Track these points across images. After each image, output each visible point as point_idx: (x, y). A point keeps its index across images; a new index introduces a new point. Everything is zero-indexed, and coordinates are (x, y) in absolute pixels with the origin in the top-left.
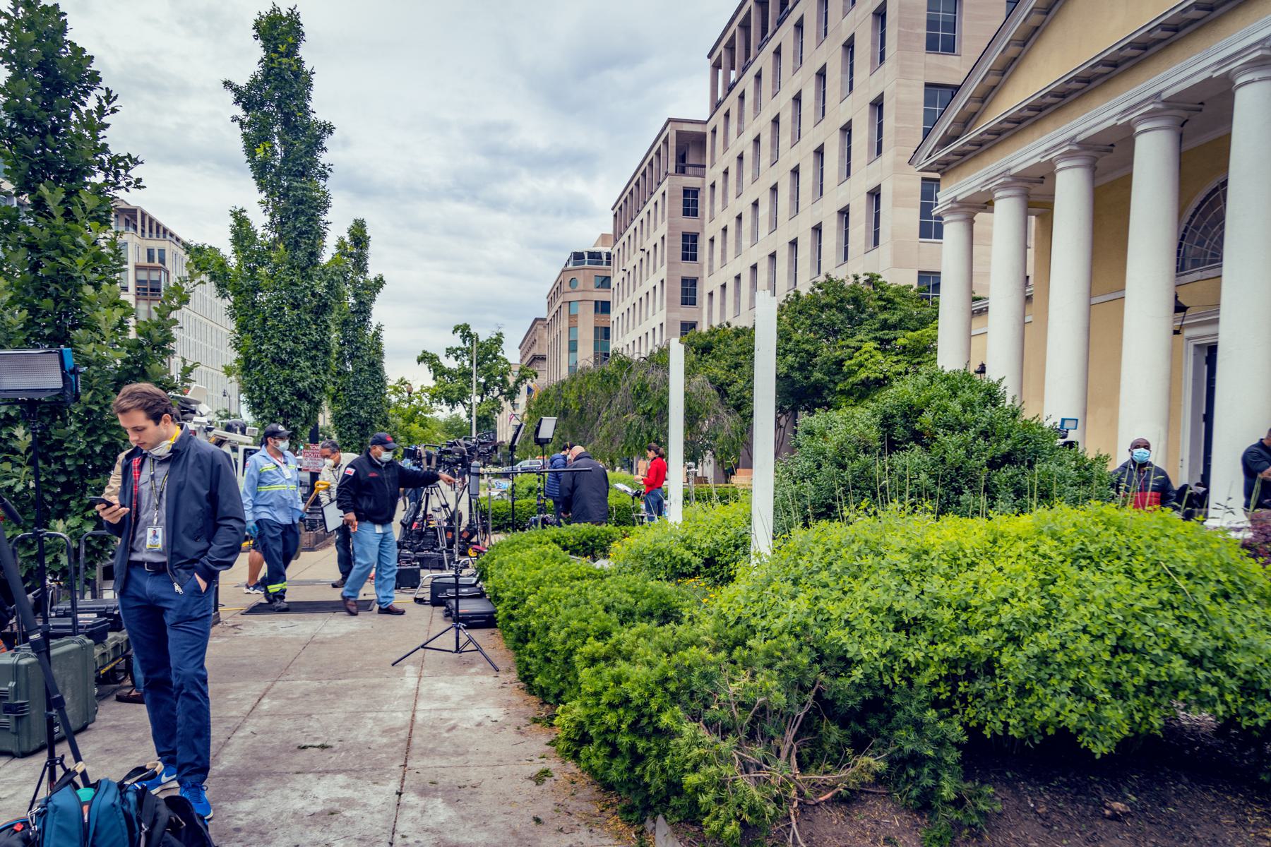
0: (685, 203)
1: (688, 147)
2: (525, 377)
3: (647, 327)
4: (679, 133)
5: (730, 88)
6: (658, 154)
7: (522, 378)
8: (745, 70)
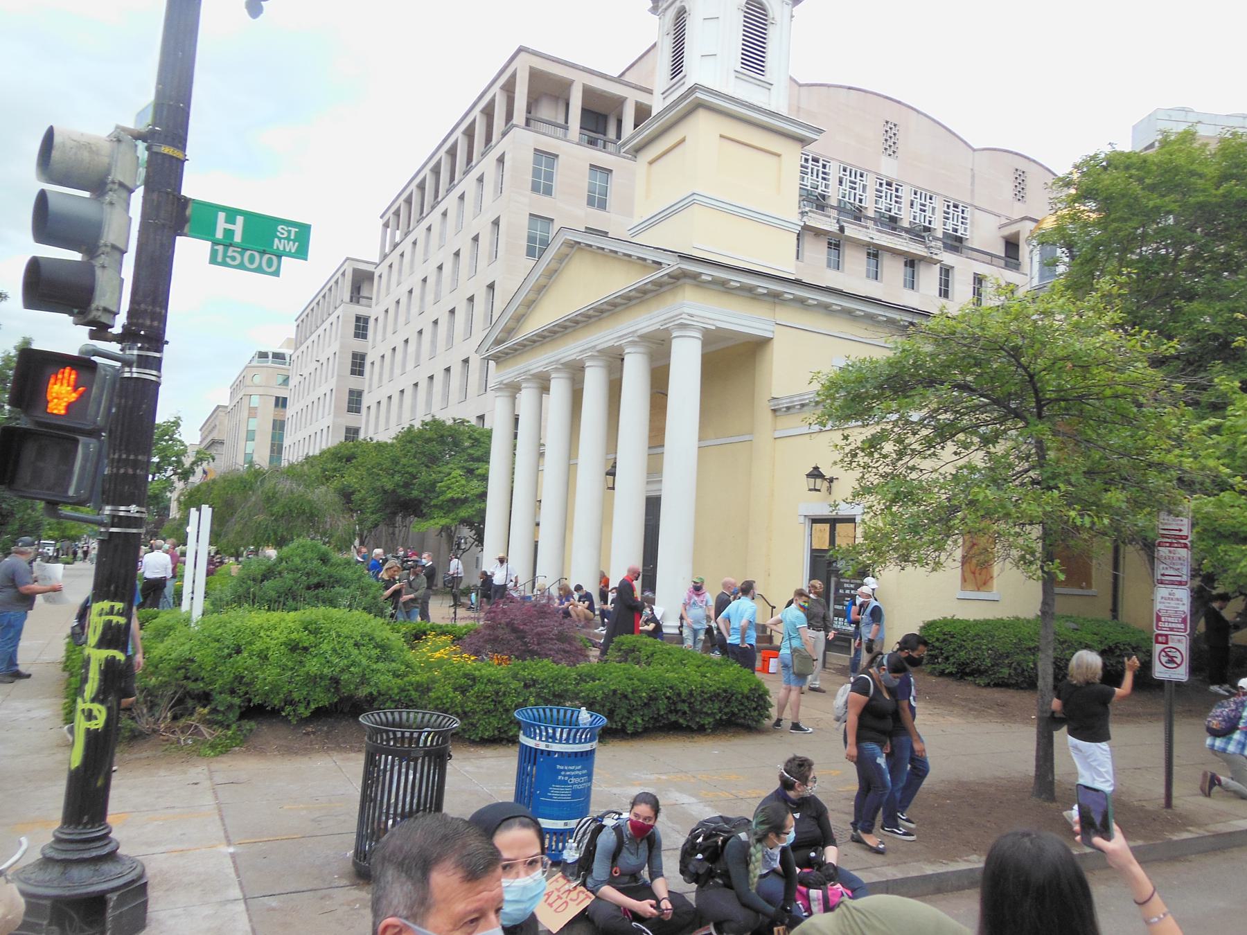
0: (357, 327)
1: (361, 282)
2: (202, 460)
3: (316, 427)
4: (535, 75)
5: (396, 246)
6: (337, 282)
7: (199, 460)
8: (406, 234)
